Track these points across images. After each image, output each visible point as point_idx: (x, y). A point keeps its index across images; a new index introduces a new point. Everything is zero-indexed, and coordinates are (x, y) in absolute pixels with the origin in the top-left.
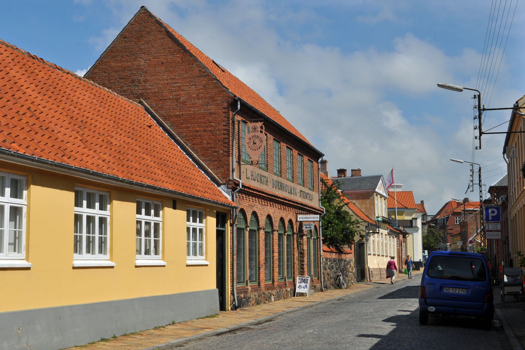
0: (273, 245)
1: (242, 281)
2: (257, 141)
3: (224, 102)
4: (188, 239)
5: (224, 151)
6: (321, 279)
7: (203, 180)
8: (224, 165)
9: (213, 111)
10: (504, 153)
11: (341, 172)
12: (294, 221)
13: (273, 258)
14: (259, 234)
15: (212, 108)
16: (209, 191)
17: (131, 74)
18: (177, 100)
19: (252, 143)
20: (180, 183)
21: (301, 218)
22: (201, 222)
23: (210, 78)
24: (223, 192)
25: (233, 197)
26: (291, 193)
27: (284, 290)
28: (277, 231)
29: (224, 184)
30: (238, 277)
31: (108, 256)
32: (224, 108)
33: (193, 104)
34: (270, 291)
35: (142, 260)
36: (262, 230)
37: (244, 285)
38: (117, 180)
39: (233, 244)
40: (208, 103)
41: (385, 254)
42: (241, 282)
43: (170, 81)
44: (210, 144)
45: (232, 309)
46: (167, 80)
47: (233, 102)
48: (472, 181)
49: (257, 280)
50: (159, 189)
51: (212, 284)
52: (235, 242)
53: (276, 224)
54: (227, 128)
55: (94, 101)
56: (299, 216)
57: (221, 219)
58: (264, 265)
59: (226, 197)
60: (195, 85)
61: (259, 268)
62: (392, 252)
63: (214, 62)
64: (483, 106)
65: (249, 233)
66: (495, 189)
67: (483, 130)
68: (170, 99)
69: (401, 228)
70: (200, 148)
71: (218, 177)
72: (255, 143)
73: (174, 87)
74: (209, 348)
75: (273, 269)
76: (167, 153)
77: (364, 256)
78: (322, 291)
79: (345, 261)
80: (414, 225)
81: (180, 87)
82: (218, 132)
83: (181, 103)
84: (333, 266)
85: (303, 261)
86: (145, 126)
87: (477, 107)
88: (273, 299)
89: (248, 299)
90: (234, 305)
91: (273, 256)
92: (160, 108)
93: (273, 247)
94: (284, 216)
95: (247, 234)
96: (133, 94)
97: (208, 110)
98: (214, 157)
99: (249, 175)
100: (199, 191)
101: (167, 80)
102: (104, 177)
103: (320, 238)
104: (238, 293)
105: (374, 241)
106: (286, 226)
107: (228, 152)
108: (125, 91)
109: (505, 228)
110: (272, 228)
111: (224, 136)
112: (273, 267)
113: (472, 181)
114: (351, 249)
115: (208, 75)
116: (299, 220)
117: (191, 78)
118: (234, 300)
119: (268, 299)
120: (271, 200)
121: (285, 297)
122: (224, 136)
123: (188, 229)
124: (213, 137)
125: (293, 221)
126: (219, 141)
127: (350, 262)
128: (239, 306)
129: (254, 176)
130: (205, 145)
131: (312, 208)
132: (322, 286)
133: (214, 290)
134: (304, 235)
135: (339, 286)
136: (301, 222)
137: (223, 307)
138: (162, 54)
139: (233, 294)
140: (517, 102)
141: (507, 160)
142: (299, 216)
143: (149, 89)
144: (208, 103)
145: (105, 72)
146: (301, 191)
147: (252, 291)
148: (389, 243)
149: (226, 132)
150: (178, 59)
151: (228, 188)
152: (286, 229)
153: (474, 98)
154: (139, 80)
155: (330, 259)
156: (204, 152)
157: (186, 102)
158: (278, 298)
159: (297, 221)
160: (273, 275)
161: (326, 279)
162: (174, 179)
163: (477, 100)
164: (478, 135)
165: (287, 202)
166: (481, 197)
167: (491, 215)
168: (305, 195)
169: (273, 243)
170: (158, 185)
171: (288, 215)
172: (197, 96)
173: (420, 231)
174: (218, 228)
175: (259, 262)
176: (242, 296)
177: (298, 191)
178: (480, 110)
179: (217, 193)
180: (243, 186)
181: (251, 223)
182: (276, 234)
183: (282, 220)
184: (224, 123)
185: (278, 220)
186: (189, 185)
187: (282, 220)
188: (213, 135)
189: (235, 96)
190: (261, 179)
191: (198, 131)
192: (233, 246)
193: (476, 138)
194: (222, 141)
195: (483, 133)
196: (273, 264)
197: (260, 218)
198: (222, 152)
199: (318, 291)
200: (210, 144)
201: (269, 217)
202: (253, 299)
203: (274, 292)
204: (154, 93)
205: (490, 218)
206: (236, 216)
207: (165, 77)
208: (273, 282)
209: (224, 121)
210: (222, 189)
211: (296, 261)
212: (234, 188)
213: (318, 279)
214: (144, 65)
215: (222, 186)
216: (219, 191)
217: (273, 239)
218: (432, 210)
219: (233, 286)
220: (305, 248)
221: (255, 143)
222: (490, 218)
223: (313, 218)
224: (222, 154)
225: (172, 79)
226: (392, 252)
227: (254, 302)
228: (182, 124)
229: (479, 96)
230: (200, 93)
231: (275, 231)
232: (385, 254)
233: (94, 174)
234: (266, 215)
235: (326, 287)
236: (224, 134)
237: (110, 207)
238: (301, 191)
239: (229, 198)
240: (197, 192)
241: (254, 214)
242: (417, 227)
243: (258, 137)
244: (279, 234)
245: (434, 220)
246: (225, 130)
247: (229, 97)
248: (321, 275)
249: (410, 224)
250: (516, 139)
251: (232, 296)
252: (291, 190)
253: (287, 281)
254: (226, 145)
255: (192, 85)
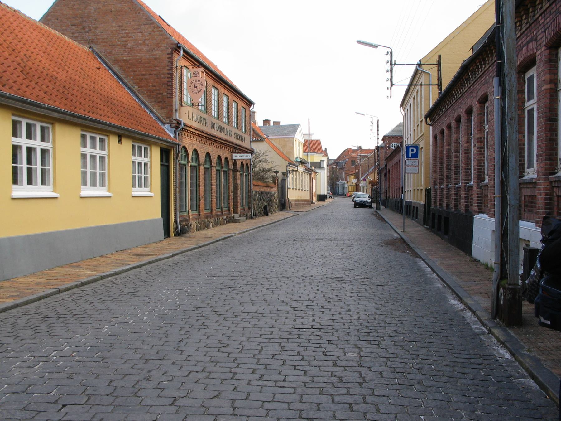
0: (211, 179)
1: (184, 210)
2: (198, 85)
3: (168, 48)
4: (134, 172)
5: (167, 94)
6: (251, 209)
7: (149, 119)
8: (168, 106)
9: (158, 56)
10: (400, 107)
11: (266, 122)
12: (229, 158)
13: (211, 191)
14: (199, 169)
15: (158, 53)
16: (153, 128)
17: (82, 21)
18: (125, 46)
19: (193, 87)
20: (125, 120)
21: (236, 156)
22: (146, 156)
23: (156, 26)
24: (166, 130)
25: (175, 134)
26: (227, 134)
27: (221, 218)
28: (215, 167)
29: (168, 123)
30: (181, 206)
31: (51, 187)
32: (168, 54)
33: (140, 50)
34: (209, 219)
35: (138, 192)
36: (202, 165)
37: (186, 214)
38: (58, 111)
39: (176, 177)
40: (154, 49)
41: (301, 189)
42: (183, 212)
43: (118, 28)
44: (155, 86)
45: (175, 235)
46: (115, 27)
47: (177, 48)
48: (372, 130)
49: (198, 210)
50: (103, 124)
51: (156, 213)
52: (178, 175)
53: (214, 160)
54: (171, 72)
55: (43, 40)
56: (234, 155)
57: (165, 154)
58: (203, 197)
59: (169, 135)
60: (142, 32)
61: (199, 199)
62: (306, 187)
63: (160, 17)
64: (395, 61)
65: (191, 168)
66: (387, 138)
67: (394, 82)
68: (118, 45)
69: (313, 168)
70: (146, 91)
71: (162, 117)
72: (196, 87)
73: (122, 34)
74: (151, 277)
75: (212, 200)
76: (115, 93)
77: (285, 190)
78: (252, 218)
79: (270, 194)
80: (321, 166)
81: (127, 34)
82: (162, 76)
83: (128, 48)
84: (261, 198)
85: (237, 194)
86: (94, 68)
87: (389, 62)
88: (211, 226)
89: (189, 226)
90: (178, 232)
91: (212, 189)
92: (109, 53)
93: (211, 181)
94: (221, 155)
95: (189, 169)
96: (84, 40)
97: (153, 55)
98: (159, 98)
99: (191, 116)
100: (144, 128)
101: (115, 27)
102: (43, 108)
103: (250, 174)
104: (180, 221)
105: (293, 178)
106: (223, 163)
107: (171, 94)
108: (76, 37)
109: (397, 168)
110: (211, 164)
111: (167, 80)
112: (212, 199)
113: (372, 130)
114: (275, 184)
115: (153, 23)
116: (233, 158)
117: (138, 25)
118: (177, 228)
119: (207, 226)
120: (210, 139)
121: (222, 224)
122: (167, 80)
123: (134, 163)
124: (158, 80)
125: (229, 159)
126: (163, 84)
127: (274, 194)
128: (182, 233)
129: (195, 118)
130: (151, 88)
131: (245, 148)
132: (251, 214)
133: (159, 219)
134: (238, 171)
135: (266, 214)
136: (235, 160)
137: (167, 233)
138: (110, 4)
139: (176, 222)
140: (420, 61)
141: (403, 112)
142: (234, 155)
143: (99, 35)
144: (154, 49)
145: (57, 19)
146: (235, 133)
147: (193, 220)
148: (304, 179)
149: (169, 76)
150: (126, 8)
151: (171, 127)
152: (223, 166)
153: (387, 54)
154: (89, 27)
155: (258, 192)
156: (150, 93)
157: (133, 48)
158: (216, 224)
159: (232, 159)
160: (212, 205)
161: (255, 208)
162: (120, 116)
163: (389, 56)
164: (389, 87)
165: (224, 142)
166: (378, 143)
167: (411, 153)
168: (240, 137)
169: (211, 178)
170: (103, 119)
171: (225, 154)
172: (144, 42)
173: (326, 170)
174: (162, 163)
175: (199, 193)
176: (185, 223)
177: (233, 133)
178: (391, 64)
179: (161, 131)
180: (185, 125)
181: (192, 160)
182: (214, 170)
183: (219, 157)
184: (168, 68)
185: (216, 157)
186: (135, 122)
187: (219, 157)
188: (158, 78)
189: (178, 43)
190: (201, 121)
191: (144, 75)
192: (176, 180)
193: (388, 88)
194: (166, 84)
195: (394, 85)
196: (211, 195)
197: (200, 155)
198: (166, 94)
199: (249, 219)
200: (155, 86)
201: (208, 154)
202: (194, 227)
203: (212, 220)
204: (104, 39)
205: (410, 156)
206: (179, 152)
207: (114, 25)
208: (212, 211)
209: (168, 66)
210: (166, 128)
211: (231, 193)
212: (177, 127)
213: (249, 208)
214: (94, 13)
215: (166, 126)
216: (163, 129)
217: (211, 174)
218: (334, 155)
219: (175, 215)
220: (239, 182)
221: (196, 87)
222: (410, 156)
223: (246, 156)
224: (166, 95)
225: (120, 26)
226: (306, 187)
227: (195, 229)
228: (129, 68)
229: (391, 53)
230: (146, 40)
231: (213, 167)
232: (301, 189)
233: (31, 104)
234: (206, 152)
235: (255, 215)
236: (168, 78)
237: (548, 325)
238: (235, 133)
239: (172, 136)
240: (142, 129)
241: (195, 151)
242: (324, 168)
243: (199, 81)
244: (217, 170)
245: (336, 162)
246: (168, 74)
247: (172, 44)
248: (251, 205)
249: (318, 165)
250: (415, 94)
251: (175, 224)
252: (227, 132)
253: (223, 210)
254: (170, 88)
255: (138, 33)
